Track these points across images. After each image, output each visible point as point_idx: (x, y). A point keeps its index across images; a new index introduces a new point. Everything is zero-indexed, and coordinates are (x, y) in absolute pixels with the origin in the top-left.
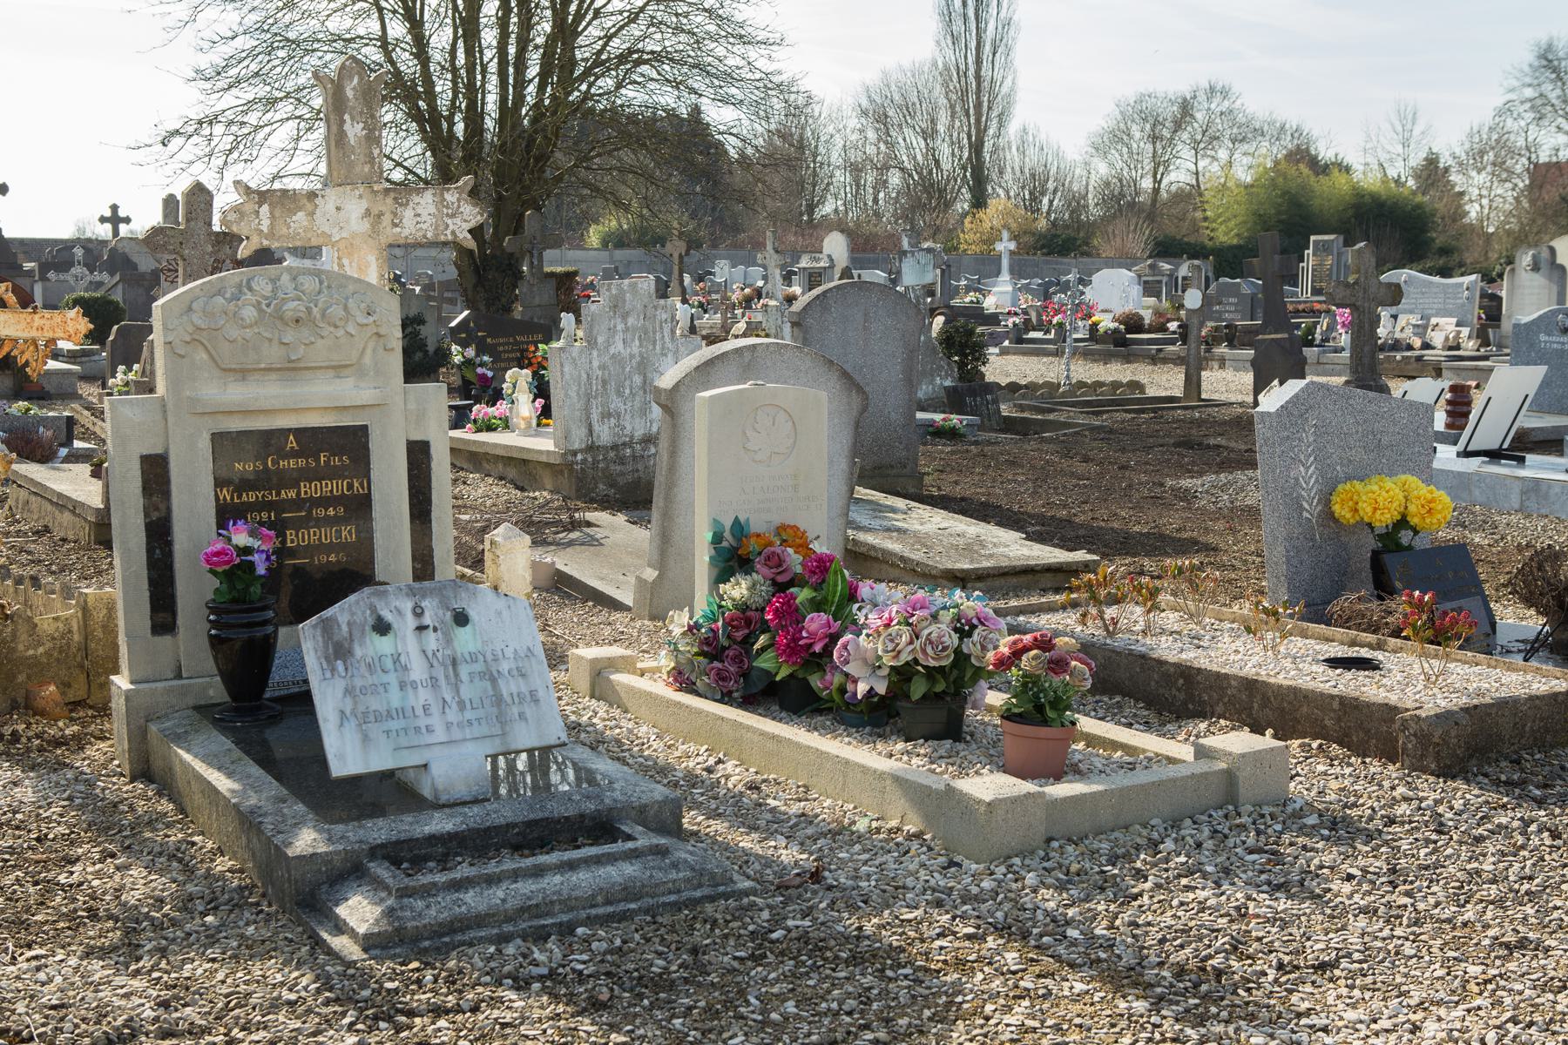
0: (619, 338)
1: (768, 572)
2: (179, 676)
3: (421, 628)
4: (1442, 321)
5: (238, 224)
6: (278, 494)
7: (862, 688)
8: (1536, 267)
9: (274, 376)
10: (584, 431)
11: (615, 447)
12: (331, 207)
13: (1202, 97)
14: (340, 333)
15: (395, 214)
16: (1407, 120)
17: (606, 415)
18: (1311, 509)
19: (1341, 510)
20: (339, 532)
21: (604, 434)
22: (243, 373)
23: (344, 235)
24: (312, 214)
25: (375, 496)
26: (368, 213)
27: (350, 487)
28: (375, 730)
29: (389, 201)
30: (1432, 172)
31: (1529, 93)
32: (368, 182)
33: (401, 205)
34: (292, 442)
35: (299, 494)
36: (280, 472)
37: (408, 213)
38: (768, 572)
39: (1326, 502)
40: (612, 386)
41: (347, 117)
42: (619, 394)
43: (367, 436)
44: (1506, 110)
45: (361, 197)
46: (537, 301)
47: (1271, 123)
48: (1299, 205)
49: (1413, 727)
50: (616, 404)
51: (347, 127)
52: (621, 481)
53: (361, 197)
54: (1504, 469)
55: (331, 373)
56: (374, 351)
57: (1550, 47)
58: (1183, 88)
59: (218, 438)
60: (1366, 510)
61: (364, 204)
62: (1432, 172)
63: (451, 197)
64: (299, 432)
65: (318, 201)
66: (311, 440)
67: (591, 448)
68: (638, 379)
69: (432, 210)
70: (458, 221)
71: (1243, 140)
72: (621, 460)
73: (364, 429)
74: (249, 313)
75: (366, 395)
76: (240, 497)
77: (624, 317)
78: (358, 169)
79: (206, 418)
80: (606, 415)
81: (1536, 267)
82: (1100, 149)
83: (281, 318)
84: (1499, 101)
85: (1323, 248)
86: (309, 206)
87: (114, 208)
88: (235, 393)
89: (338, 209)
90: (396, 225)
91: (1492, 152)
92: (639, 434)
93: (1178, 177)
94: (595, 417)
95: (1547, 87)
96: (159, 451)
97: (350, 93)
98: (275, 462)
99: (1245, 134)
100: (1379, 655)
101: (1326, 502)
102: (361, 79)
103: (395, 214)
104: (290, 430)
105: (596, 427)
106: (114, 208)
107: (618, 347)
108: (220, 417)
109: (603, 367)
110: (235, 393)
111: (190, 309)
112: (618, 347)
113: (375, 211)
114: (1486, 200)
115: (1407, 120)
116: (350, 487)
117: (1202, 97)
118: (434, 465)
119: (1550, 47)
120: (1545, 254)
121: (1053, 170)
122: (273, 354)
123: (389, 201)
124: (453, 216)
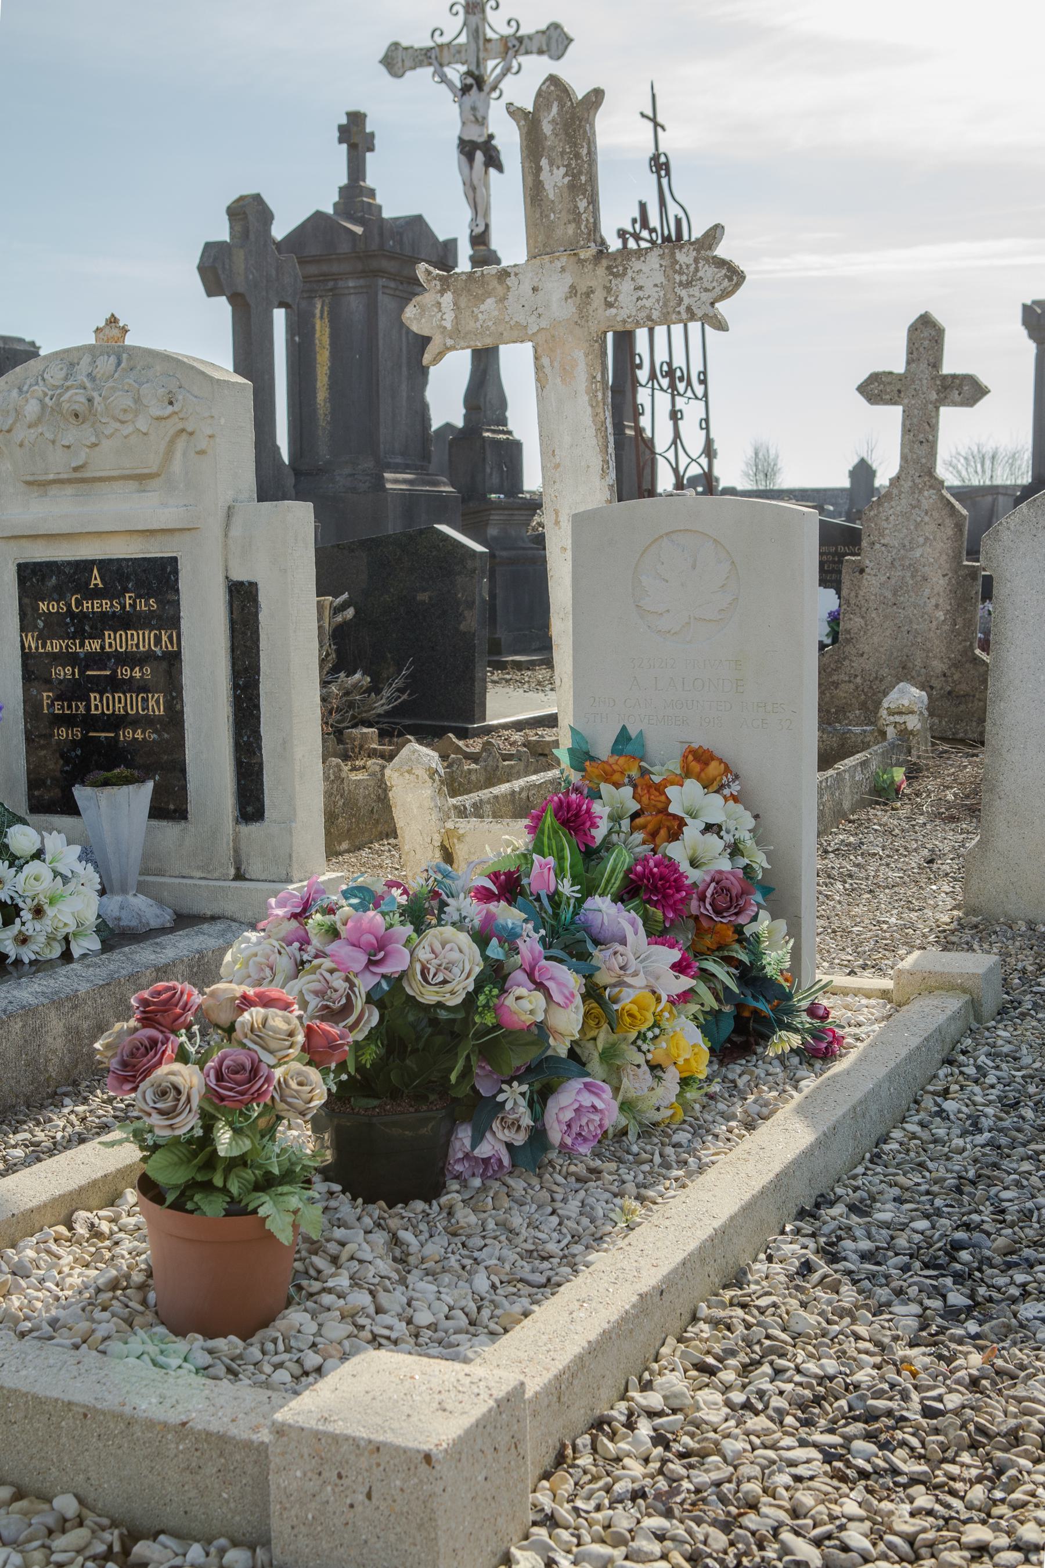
5: (419, 321)
6: (82, 645)
12: (526, 287)
14: (128, 429)
15: (608, 290)
20: (145, 700)
23: (544, 324)
24: (503, 299)
26: (573, 290)
27: (158, 640)
29: (601, 271)
32: (572, 249)
33: (616, 276)
34: (96, 581)
35: (102, 647)
37: (626, 287)
41: (544, 162)
43: (176, 572)
45: (563, 269)
51: (544, 176)
53: (563, 269)
55: (133, 485)
56: (184, 454)
61: (568, 279)
64: (104, 565)
65: (511, 281)
66: (120, 574)
69: (660, 278)
70: (695, 291)
73: (174, 560)
76: (44, 646)
78: (559, 232)
79: (12, 543)
86: (500, 290)
87: (926, 336)
89: (535, 289)
90: (609, 305)
98: (79, 603)
102: (562, 106)
103: (608, 290)
104: (93, 562)
106: (926, 336)
108: (24, 543)
113: (582, 288)
116: (158, 640)
118: (262, 617)
122: (58, 464)
123: (601, 271)
124: (688, 284)
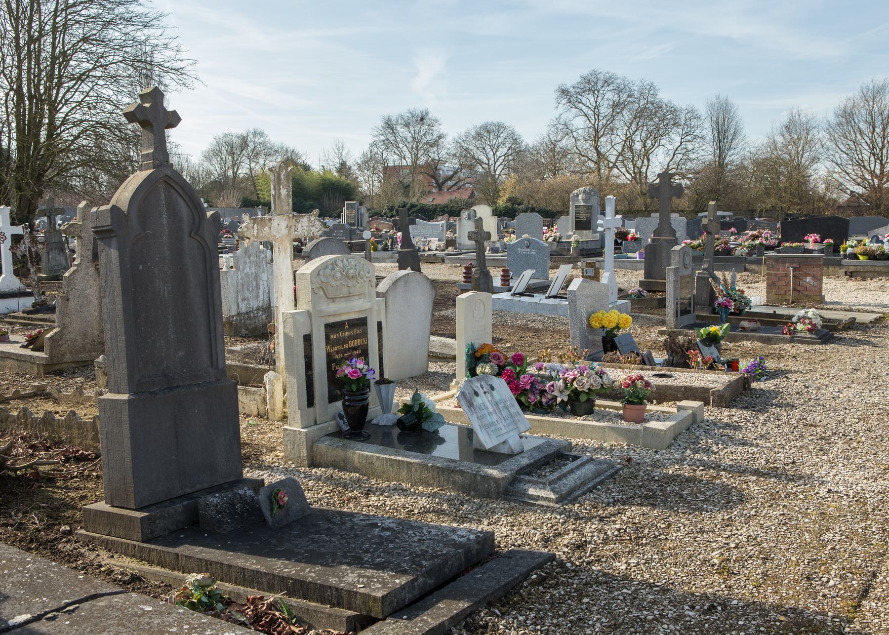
0: (247, 266)
1: (497, 362)
2: (316, 424)
3: (485, 393)
4: (432, 239)
7: (559, 400)
8: (469, 218)
9: (343, 300)
10: (236, 307)
11: (247, 313)
13: (251, 136)
16: (340, 149)
17: (244, 299)
18: (585, 323)
19: (595, 324)
21: (243, 309)
22: (333, 300)
24: (270, 228)
25: (369, 344)
28: (489, 430)
30: (343, 168)
31: (382, 138)
36: (344, 338)
37: (300, 226)
38: (497, 362)
39: (589, 321)
40: (245, 287)
42: (248, 290)
44: (373, 145)
46: (53, 241)
47: (282, 148)
48: (299, 184)
49: (717, 393)
50: (247, 294)
52: (250, 327)
54: (523, 299)
57: (389, 120)
58: (242, 131)
59: (327, 326)
60: (605, 323)
61: (286, 223)
62: (343, 168)
63: (312, 219)
67: (239, 314)
68: (254, 283)
71: (270, 155)
72: (250, 318)
74: (338, 275)
75: (367, 305)
77: (249, 257)
80: (244, 299)
81: (469, 218)
82: (208, 158)
83: (348, 277)
84: (371, 141)
85: (350, 207)
88: (332, 307)
91: (369, 162)
92: (255, 307)
93: (243, 171)
94: (240, 300)
95: (389, 136)
96: (308, 333)
97: (282, 177)
99: (271, 152)
100: (672, 373)
101: (589, 321)
105: (240, 305)
107: (247, 270)
109: (242, 279)
110: (332, 307)
111: (319, 274)
112: (247, 270)
114: (369, 184)
115: (340, 149)
117: (251, 136)
119: (389, 120)
120: (472, 213)
121: (185, 167)
